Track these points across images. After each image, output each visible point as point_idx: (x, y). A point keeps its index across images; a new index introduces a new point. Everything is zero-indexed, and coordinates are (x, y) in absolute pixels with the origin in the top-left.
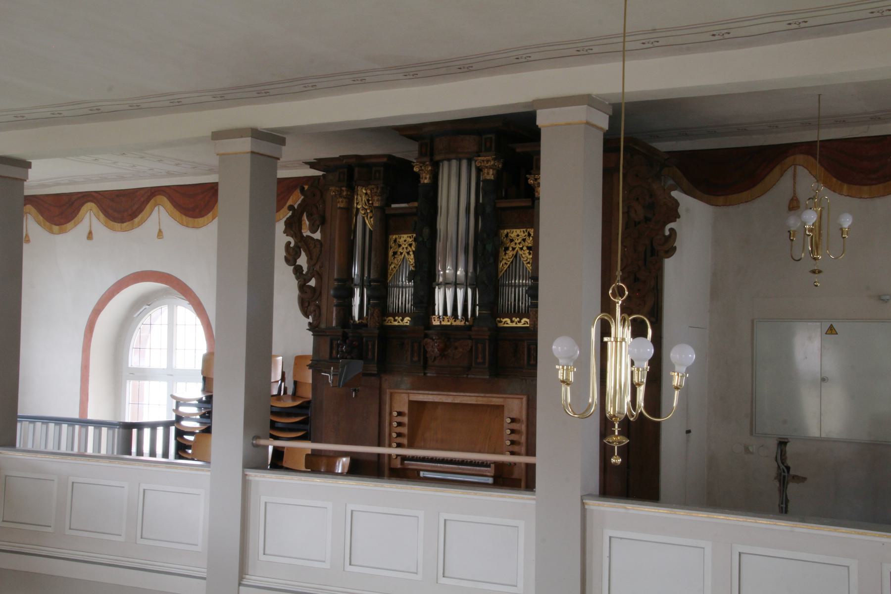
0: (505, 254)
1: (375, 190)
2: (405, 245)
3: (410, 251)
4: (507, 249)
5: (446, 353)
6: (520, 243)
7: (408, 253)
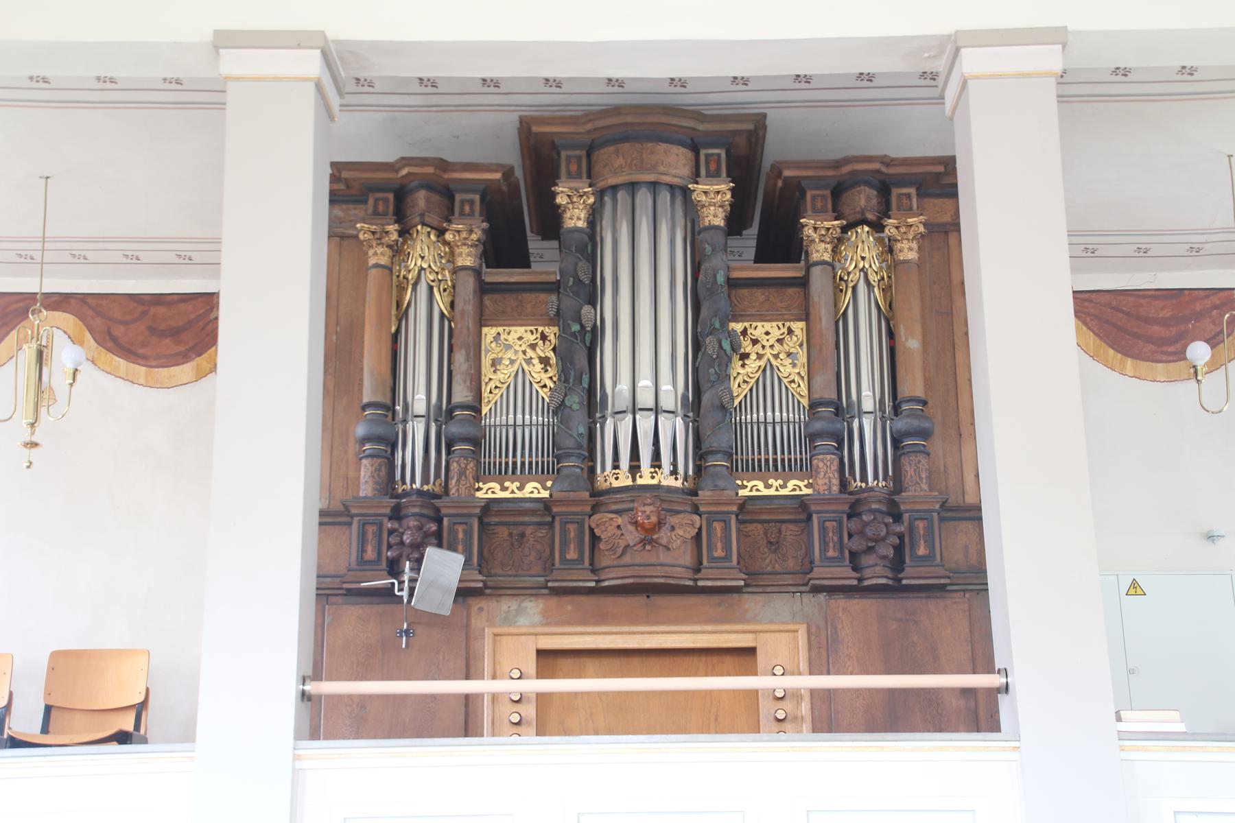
0: (743, 366)
1: (464, 235)
4: (745, 356)
5: (655, 537)
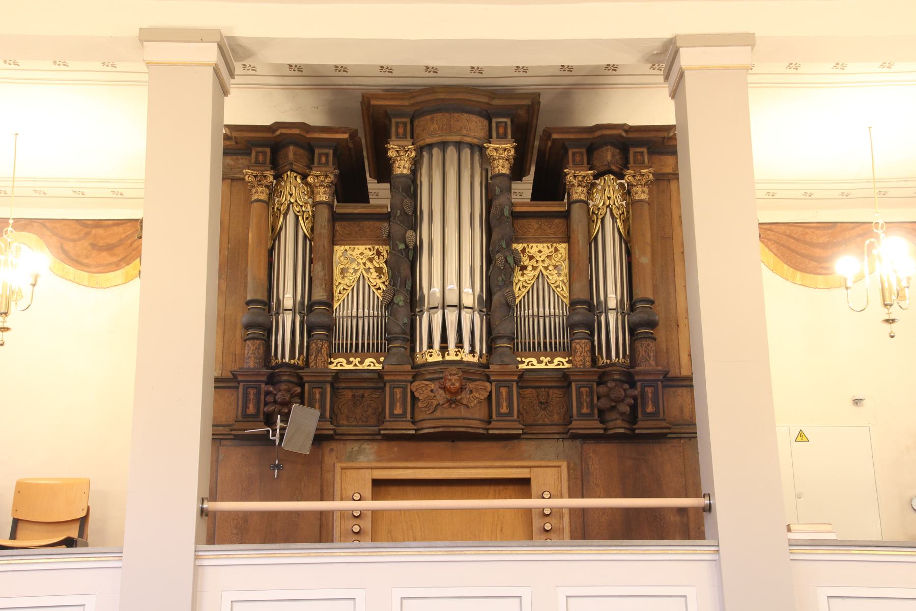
2: (362, 259)
3: (369, 268)
4: (524, 268)
6: (543, 261)
7: (368, 270)
